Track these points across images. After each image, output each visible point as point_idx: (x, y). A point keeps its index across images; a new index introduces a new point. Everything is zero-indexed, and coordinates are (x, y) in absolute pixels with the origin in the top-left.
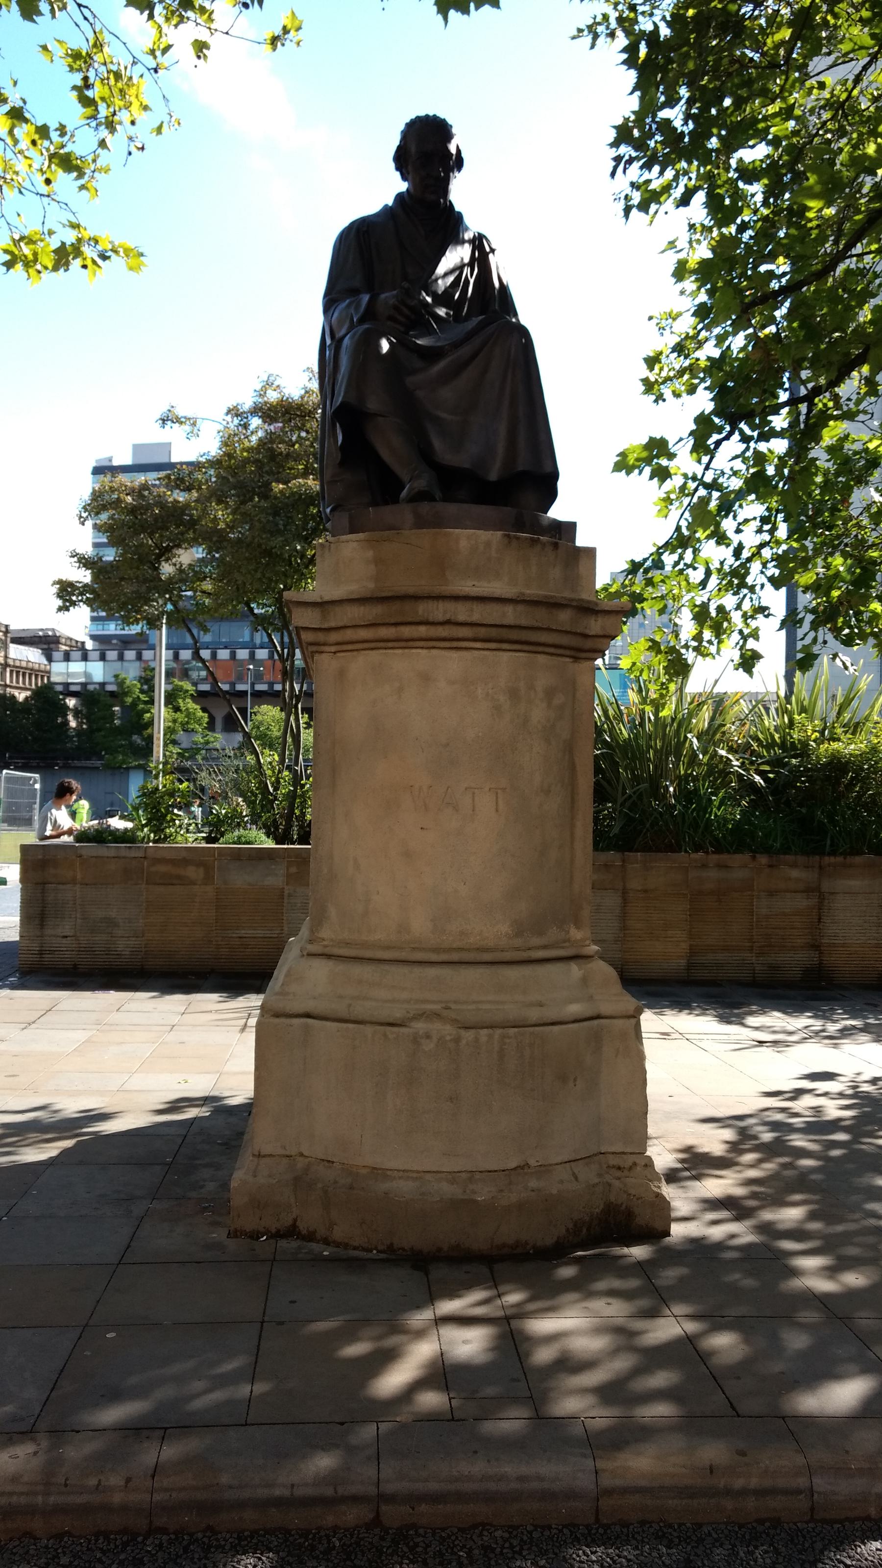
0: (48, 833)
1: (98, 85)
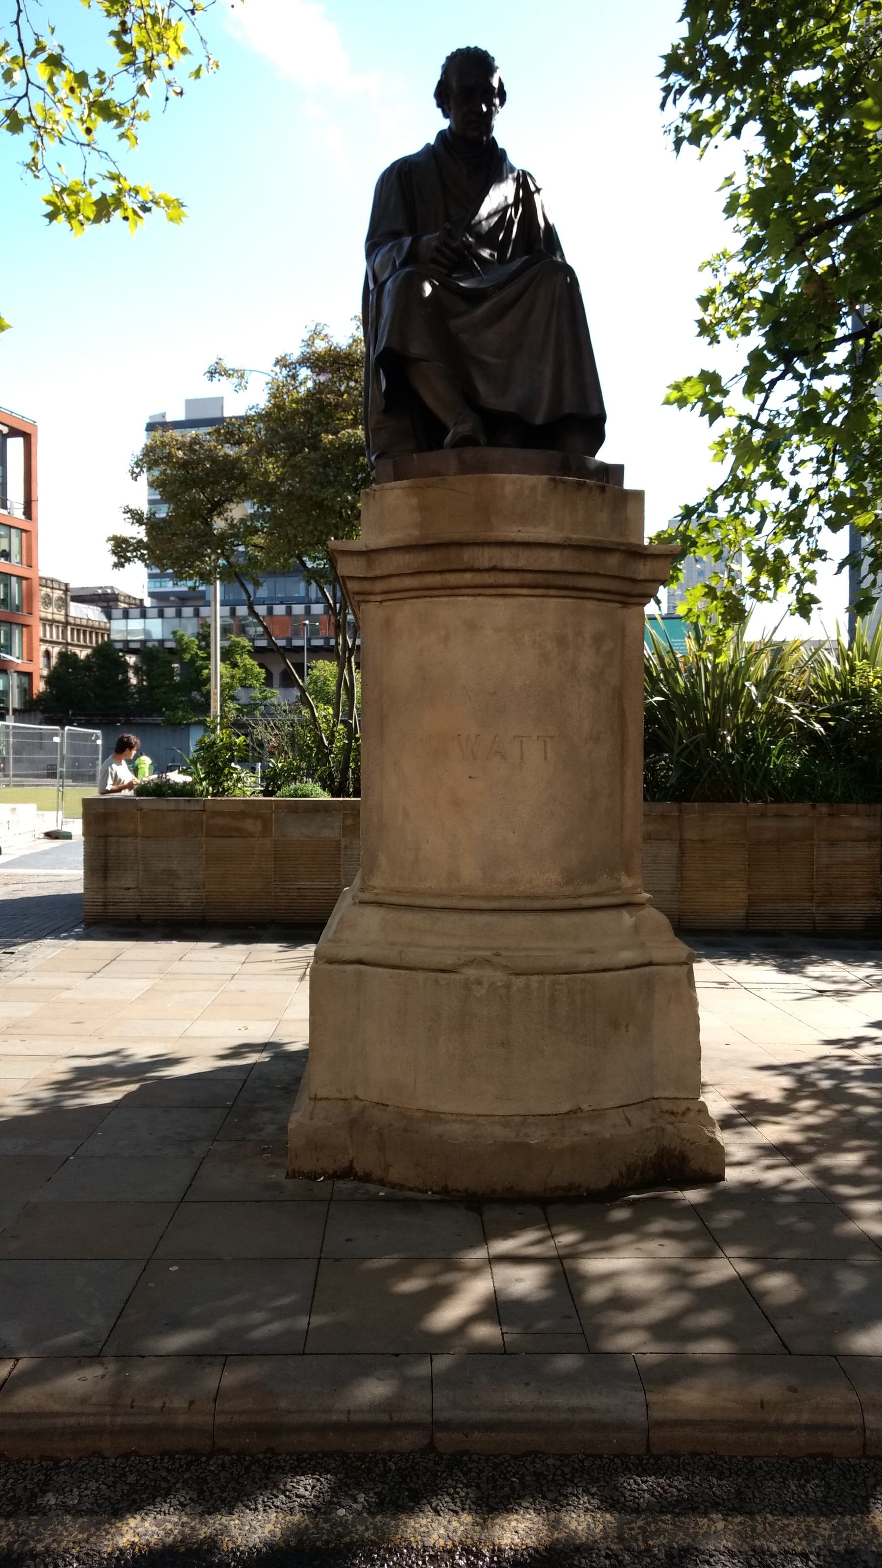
0: (109, 787)
1: (135, 29)
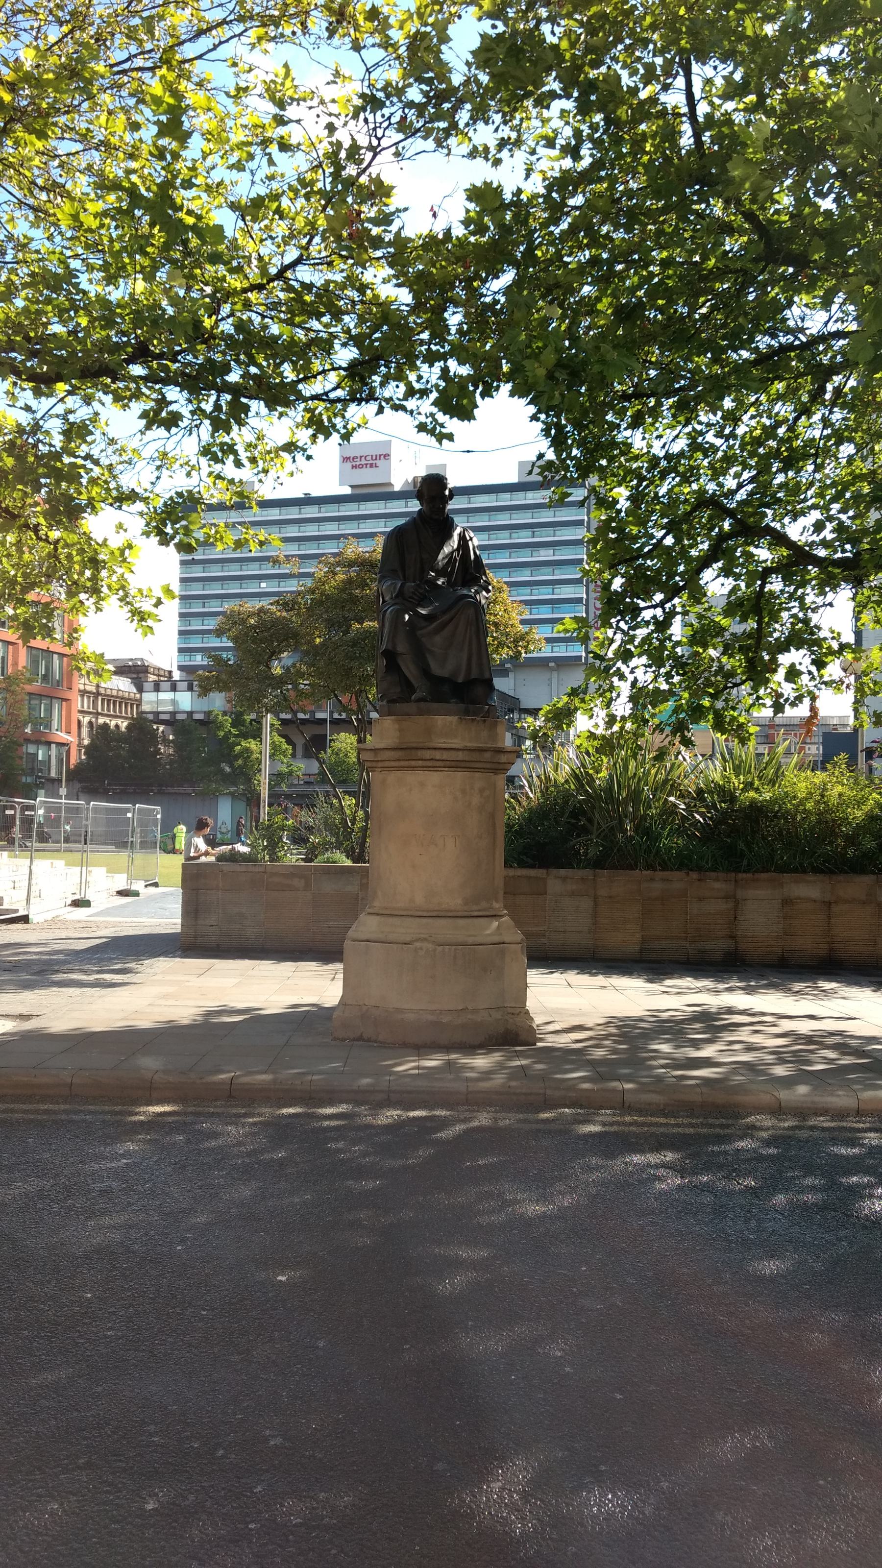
0: (192, 854)
